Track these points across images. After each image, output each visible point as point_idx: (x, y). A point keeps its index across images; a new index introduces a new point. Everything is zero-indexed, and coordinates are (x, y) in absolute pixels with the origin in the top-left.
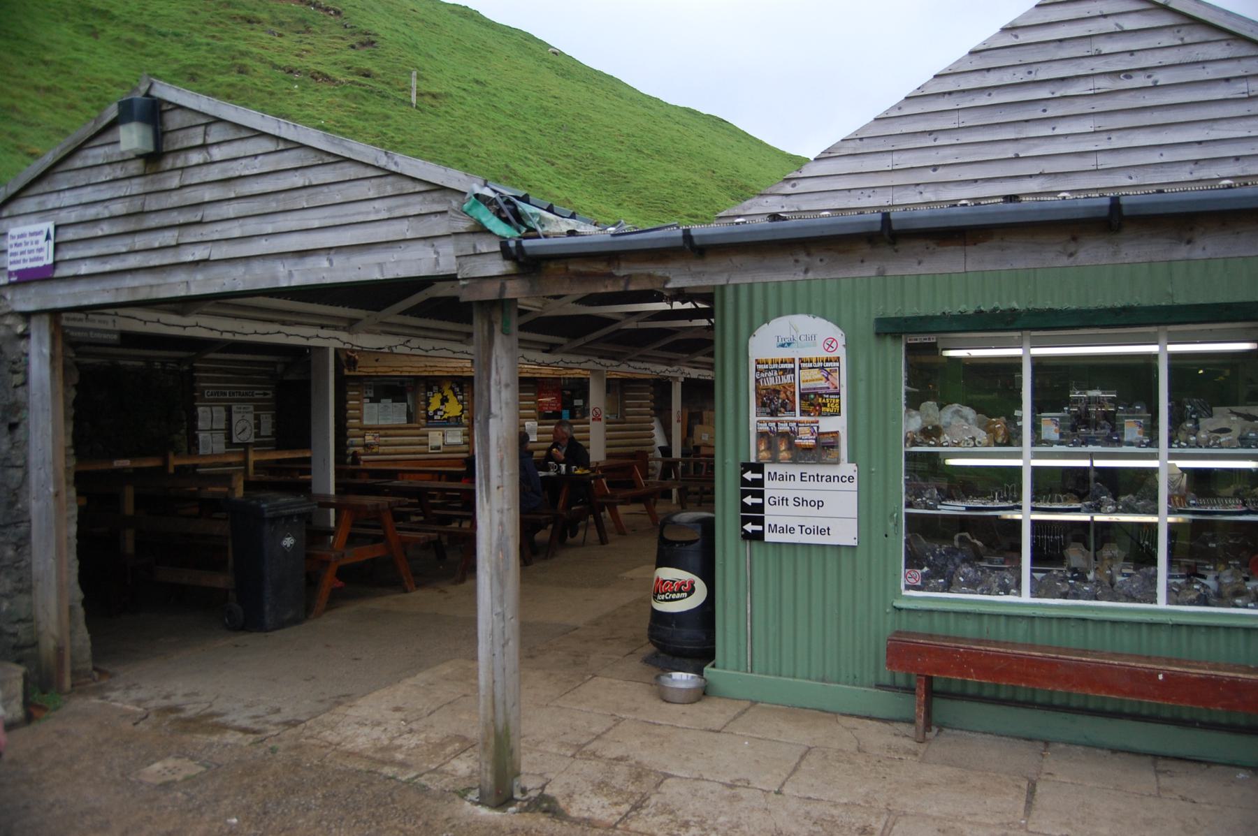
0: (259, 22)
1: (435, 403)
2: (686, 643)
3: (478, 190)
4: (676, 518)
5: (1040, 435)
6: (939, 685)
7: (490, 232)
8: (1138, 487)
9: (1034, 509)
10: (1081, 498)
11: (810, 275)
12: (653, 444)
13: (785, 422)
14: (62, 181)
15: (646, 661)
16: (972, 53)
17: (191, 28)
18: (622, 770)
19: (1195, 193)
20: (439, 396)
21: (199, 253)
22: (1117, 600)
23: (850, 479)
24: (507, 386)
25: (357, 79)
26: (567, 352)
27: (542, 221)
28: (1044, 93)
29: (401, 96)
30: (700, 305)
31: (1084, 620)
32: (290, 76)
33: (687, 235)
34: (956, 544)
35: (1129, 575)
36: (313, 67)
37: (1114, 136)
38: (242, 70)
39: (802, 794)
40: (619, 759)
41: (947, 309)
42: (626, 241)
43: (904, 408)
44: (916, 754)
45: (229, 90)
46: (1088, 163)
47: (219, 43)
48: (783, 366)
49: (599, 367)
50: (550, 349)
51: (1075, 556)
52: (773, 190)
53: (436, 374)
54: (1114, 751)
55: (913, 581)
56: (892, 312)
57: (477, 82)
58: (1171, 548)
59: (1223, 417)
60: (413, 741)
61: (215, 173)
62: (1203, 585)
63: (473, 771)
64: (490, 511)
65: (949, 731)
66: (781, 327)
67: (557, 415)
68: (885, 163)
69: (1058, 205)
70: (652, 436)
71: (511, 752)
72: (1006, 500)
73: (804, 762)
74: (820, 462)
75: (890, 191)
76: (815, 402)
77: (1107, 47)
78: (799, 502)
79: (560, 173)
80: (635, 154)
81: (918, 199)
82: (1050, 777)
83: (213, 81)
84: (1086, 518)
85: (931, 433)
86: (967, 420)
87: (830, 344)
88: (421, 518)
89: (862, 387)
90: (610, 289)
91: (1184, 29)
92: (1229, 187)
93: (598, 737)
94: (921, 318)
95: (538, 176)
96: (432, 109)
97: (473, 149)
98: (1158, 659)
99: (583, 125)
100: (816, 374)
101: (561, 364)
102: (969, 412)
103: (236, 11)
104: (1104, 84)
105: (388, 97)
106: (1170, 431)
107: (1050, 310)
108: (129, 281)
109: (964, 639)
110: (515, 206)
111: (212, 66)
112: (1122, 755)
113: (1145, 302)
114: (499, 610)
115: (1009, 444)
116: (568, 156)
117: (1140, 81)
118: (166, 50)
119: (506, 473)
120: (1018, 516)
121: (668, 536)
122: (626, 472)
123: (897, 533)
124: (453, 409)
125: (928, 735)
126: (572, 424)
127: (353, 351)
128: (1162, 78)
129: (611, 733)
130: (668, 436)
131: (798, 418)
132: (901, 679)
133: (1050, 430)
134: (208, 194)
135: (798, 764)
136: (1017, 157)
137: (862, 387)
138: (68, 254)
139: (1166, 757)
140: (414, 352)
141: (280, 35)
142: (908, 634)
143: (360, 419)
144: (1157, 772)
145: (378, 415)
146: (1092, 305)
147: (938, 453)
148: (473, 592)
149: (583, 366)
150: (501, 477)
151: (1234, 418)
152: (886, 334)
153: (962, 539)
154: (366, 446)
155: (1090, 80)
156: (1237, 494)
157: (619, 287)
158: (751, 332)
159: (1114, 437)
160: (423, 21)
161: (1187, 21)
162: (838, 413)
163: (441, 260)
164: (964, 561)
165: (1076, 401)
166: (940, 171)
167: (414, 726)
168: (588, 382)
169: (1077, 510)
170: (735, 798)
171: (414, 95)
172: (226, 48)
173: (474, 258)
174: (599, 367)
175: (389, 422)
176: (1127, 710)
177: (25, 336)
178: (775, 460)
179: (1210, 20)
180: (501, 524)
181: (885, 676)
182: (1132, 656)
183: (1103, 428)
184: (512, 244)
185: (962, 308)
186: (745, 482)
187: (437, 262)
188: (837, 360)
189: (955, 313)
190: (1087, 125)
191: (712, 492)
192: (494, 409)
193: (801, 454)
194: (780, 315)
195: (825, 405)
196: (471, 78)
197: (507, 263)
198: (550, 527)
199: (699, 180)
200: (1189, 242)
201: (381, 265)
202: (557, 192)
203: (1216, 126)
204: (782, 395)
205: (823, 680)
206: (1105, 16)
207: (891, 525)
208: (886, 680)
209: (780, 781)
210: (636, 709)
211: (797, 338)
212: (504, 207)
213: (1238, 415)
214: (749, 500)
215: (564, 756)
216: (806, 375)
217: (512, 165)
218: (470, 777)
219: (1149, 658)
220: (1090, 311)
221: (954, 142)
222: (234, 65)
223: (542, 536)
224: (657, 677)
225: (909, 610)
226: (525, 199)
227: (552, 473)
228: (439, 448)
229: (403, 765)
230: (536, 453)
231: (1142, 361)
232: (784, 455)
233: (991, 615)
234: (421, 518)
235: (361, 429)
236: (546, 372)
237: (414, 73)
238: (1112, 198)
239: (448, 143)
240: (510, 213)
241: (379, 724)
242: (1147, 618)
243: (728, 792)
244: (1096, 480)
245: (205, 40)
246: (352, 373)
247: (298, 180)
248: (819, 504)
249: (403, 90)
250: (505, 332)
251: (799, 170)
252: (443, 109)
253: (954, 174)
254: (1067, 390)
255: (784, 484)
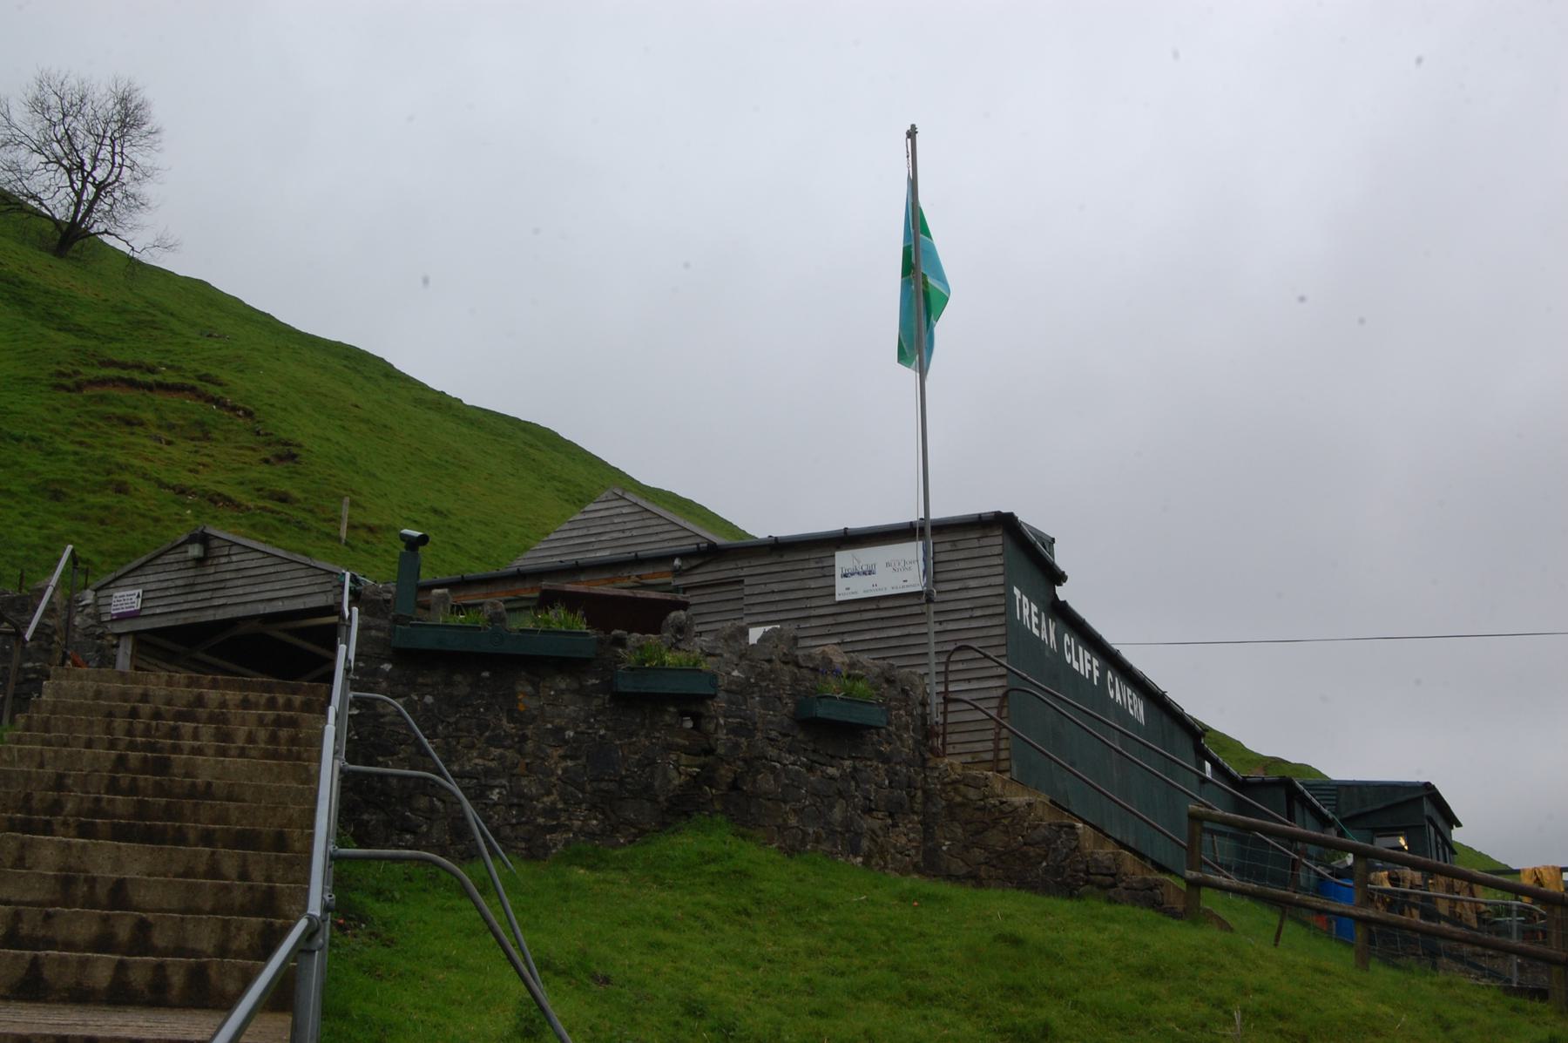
0: (141, 424)
14: (148, 570)
17: (52, 431)
21: (222, 601)
25: (269, 504)
29: (326, 528)
32: (181, 498)
36: (212, 487)
38: (121, 489)
45: (103, 514)
47: (90, 452)
61: (233, 567)
83: (82, 501)
96: (367, 547)
103: (111, 409)
105: (309, 529)
108: (183, 615)
111: (81, 482)
118: (22, 460)
134: (228, 576)
138: (149, 604)
141: (169, 443)
160: (367, 421)
171: (344, 528)
172: (102, 459)
177: (117, 646)
222: (110, 482)
237: (347, 500)
245: (71, 448)
247: (272, 570)
249: (331, 520)
252: (382, 546)
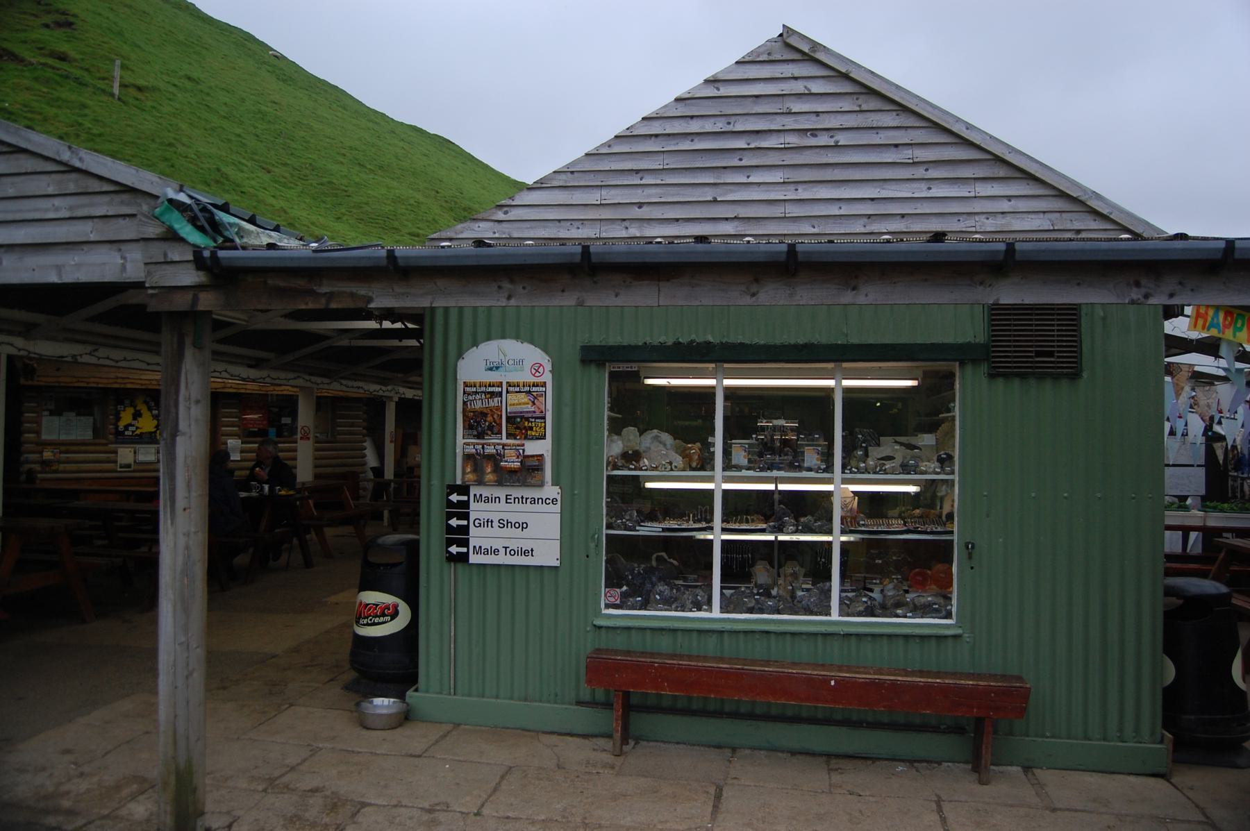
1: (126, 417)
2: (389, 668)
3: (171, 194)
4: (380, 541)
5: (730, 460)
6: (637, 700)
7: (182, 240)
8: (810, 509)
9: (724, 530)
10: (766, 520)
11: (513, 302)
12: (365, 464)
13: (492, 444)
15: (347, 688)
16: (678, 100)
18: (316, 802)
19: (860, 244)
20: (130, 411)
22: (796, 613)
23: (554, 501)
24: (197, 402)
25: (50, 61)
26: (276, 368)
27: (241, 232)
28: (740, 143)
29: (101, 84)
30: (410, 326)
31: (767, 632)
33: (391, 253)
34: (654, 563)
35: (808, 590)
37: (800, 188)
39: (501, 814)
40: (314, 791)
41: (648, 340)
42: (328, 258)
43: (606, 433)
44: (612, 767)
46: (777, 211)
48: (491, 389)
49: (309, 384)
50: (256, 364)
51: (762, 574)
52: (485, 215)
53: (129, 386)
54: (794, 753)
55: (612, 599)
56: (597, 340)
57: (189, 78)
58: (843, 564)
59: (888, 446)
60: (84, 785)
62: (870, 598)
63: (151, 814)
64: (175, 534)
65: (645, 743)
66: (490, 350)
67: (262, 433)
68: (593, 197)
69: (742, 248)
70: (365, 456)
71: (195, 790)
72: (699, 521)
73: (505, 782)
74: (525, 484)
75: (598, 224)
76: (521, 426)
77: (797, 107)
78: (504, 524)
79: (276, 182)
80: (357, 168)
81: (624, 234)
82: (735, 781)
84: (771, 538)
85: (631, 457)
86: (665, 445)
87: (537, 368)
88: (105, 542)
89: (567, 411)
90: (311, 306)
91: (862, 97)
92: (888, 241)
93: (292, 769)
94: (624, 347)
95: (253, 183)
97: (181, 149)
98: (830, 667)
99: (302, 134)
100: (523, 398)
101: (268, 380)
102: (667, 438)
104: (793, 140)
105: (86, 85)
106: (843, 458)
107: (742, 344)
109: (660, 655)
110: (212, 214)
112: (800, 757)
113: (824, 341)
114: (183, 639)
115: (702, 468)
116: (285, 165)
117: (823, 140)
119: (194, 494)
120: (711, 537)
121: (371, 559)
122: (335, 492)
123: (598, 554)
124: (147, 424)
125: (625, 748)
126: (276, 443)
127: (31, 359)
128: (843, 139)
129: (307, 764)
130: (381, 456)
131: (504, 440)
132: (600, 694)
133: (740, 457)
135: (499, 784)
136: (715, 201)
137: (567, 411)
139: (838, 756)
140: (102, 362)
142: (607, 651)
143: (38, 433)
144: (830, 770)
145: (58, 429)
146: (778, 342)
147: (638, 476)
148: (155, 622)
149: (292, 382)
150: (188, 498)
151: (897, 447)
152: (591, 361)
153: (659, 559)
154: (44, 463)
155: (782, 135)
156: (900, 517)
157: (320, 305)
158: (460, 355)
159: (795, 463)
161: (863, 91)
162: (543, 437)
163: (129, 266)
164: (660, 579)
165: (763, 429)
166: (645, 209)
167: (86, 769)
168: (297, 401)
169: (762, 531)
170: (435, 822)
171: (116, 85)
173: (164, 267)
174: (309, 384)
175: (72, 437)
176: (804, 714)
178: (480, 482)
179: (883, 92)
180: (187, 548)
181: (585, 693)
182: (714, 659)
183: (786, 454)
184: (207, 254)
185: (662, 339)
186: (450, 504)
187: (124, 267)
188: (544, 385)
189: (655, 344)
190: (777, 176)
191: (417, 514)
192: (182, 425)
193: (507, 477)
194: (489, 338)
195: (531, 428)
196: (182, 73)
197: (200, 273)
198: (251, 550)
199: (421, 199)
200: (854, 289)
201: (59, 268)
202: (273, 201)
203: (887, 186)
204: (489, 418)
205: (526, 700)
206: (796, 78)
207: (592, 545)
208: (588, 698)
209: (479, 803)
210: (334, 738)
211: (506, 361)
212: (200, 215)
213: (901, 444)
214: (454, 522)
215: (255, 791)
216: (513, 398)
217: (223, 169)
218: (148, 820)
219: (823, 666)
220: (775, 347)
221: (659, 182)
223: (242, 560)
224: (358, 704)
225: (608, 628)
226: (225, 208)
227: (254, 494)
228: (129, 466)
229: (70, 813)
230: (237, 473)
231: (823, 394)
232: (490, 477)
233: (731, 632)
234: (105, 542)
235: (37, 444)
236: (252, 388)
237: (118, 62)
238: (789, 245)
239: (153, 140)
240: (205, 220)
241: (44, 769)
242: (823, 629)
243: (426, 817)
244: (780, 502)
246: (30, 383)
248: (524, 526)
249: (104, 79)
250: (198, 346)
251: (512, 198)
252: (149, 103)
253: (657, 213)
254: (756, 419)
255: (490, 506)
